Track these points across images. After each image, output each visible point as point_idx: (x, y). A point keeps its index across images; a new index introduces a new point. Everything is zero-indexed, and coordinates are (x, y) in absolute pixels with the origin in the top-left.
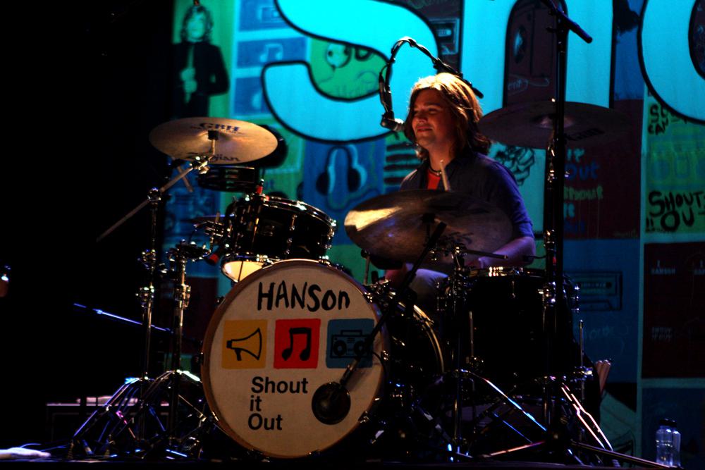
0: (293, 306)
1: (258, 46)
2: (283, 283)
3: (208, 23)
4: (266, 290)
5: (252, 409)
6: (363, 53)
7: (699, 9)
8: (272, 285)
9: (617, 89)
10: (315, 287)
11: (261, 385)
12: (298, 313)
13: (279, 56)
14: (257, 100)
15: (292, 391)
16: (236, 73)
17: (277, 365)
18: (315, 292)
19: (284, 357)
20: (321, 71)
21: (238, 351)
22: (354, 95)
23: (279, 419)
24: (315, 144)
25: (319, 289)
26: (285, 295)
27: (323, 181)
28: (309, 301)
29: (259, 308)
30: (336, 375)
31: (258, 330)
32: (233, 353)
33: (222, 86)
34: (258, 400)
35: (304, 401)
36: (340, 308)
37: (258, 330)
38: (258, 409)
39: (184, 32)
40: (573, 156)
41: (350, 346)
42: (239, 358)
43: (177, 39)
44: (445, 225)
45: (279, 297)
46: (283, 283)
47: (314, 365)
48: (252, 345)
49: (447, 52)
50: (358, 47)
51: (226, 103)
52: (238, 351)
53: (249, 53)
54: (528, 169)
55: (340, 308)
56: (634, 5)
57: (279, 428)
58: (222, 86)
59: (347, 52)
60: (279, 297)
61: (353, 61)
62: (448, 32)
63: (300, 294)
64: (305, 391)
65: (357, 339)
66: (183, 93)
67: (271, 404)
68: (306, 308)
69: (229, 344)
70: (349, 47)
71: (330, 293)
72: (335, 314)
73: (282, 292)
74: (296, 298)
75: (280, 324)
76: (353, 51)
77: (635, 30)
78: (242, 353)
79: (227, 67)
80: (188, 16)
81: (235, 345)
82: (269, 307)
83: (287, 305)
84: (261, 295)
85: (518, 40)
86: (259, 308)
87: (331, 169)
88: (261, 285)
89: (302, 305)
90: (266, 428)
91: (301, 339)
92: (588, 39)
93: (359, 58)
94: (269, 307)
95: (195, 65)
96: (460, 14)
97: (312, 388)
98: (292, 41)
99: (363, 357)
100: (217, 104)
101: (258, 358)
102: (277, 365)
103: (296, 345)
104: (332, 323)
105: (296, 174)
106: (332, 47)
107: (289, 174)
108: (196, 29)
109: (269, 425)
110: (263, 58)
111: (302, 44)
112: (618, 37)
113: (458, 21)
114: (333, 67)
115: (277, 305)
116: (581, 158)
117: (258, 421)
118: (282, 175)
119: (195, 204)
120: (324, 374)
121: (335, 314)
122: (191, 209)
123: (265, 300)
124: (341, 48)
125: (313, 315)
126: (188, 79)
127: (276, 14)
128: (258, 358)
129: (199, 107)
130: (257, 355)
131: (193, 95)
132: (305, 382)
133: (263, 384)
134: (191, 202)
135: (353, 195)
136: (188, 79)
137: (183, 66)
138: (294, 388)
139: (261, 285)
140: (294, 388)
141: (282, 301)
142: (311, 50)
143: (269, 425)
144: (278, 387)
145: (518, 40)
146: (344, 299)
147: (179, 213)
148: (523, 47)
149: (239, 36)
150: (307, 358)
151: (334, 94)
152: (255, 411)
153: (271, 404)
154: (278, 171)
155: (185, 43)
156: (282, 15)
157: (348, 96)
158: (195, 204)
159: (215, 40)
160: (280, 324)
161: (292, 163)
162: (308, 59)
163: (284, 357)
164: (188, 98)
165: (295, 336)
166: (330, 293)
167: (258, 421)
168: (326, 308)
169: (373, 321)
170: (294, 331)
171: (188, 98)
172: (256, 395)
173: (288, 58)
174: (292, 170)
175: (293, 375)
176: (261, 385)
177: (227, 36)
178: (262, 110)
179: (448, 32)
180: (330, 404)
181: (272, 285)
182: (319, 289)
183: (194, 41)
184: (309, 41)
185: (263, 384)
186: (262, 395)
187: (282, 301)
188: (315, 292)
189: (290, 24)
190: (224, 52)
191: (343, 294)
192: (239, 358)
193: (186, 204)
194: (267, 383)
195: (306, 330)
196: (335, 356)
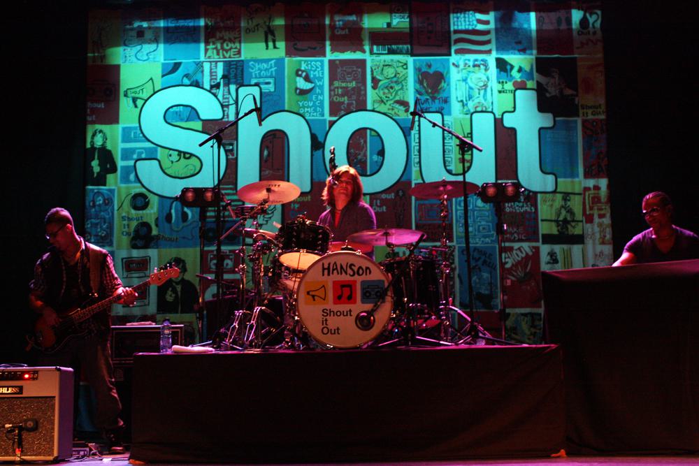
0: (341, 274)
1: (133, 151)
2: (335, 263)
3: (105, 138)
4: (326, 266)
5: (323, 324)
6: (188, 156)
7: (351, 142)
8: (329, 264)
9: (314, 177)
10: (352, 265)
11: (327, 313)
12: (344, 278)
13: (143, 156)
14: (132, 177)
15: (344, 316)
16: (120, 164)
17: (335, 303)
18: (353, 267)
19: (338, 299)
20: (166, 164)
21: (313, 296)
22: (183, 176)
23: (338, 329)
24: (165, 199)
25: (354, 266)
26: (337, 269)
27: (168, 218)
28: (350, 271)
29: (323, 275)
30: (368, 307)
31: (324, 286)
32: (311, 297)
33: (113, 169)
34: (326, 320)
35: (351, 320)
36: (366, 274)
37: (324, 286)
38: (326, 324)
39: (92, 143)
40: (294, 207)
41: (374, 293)
42: (314, 300)
43: (88, 146)
44: (544, 236)
45: (333, 270)
46: (335, 263)
47: (355, 302)
48: (321, 293)
49: (230, 157)
50: (185, 153)
51: (116, 178)
52: (313, 296)
53: (127, 154)
54: (273, 212)
55: (366, 274)
56: (321, 139)
57: (339, 334)
58: (113, 169)
59: (179, 155)
60: (333, 270)
61: (182, 159)
62: (231, 147)
63: (345, 267)
64: (351, 315)
65: (377, 290)
66: (93, 173)
67: (333, 322)
68: (348, 275)
69: (308, 293)
70: (180, 152)
71: (360, 268)
72: (364, 277)
73: (335, 267)
74: (342, 270)
75: (335, 283)
76: (182, 155)
77: (321, 150)
78: (316, 297)
79: (115, 160)
80: (94, 135)
81: (311, 293)
82: (329, 274)
83: (338, 274)
84: (324, 269)
85: (266, 153)
86: (323, 275)
87: (173, 211)
88: (323, 264)
89: (346, 273)
90: (331, 333)
91: (346, 290)
92: (481, 151)
93: (185, 158)
94: (329, 274)
95: (98, 159)
96: (237, 139)
97: (354, 314)
98: (150, 149)
99: (381, 296)
100: (110, 178)
101: (324, 300)
102: (335, 303)
103: (344, 293)
104: (363, 282)
105: (154, 213)
106: (171, 152)
107: (151, 214)
108: (98, 141)
109: (333, 332)
110: (135, 157)
111: (156, 151)
112: (314, 153)
113: (235, 142)
114: (172, 162)
115: (333, 273)
116: (298, 208)
117: (326, 330)
118: (147, 214)
119: (101, 227)
120: (360, 307)
121: (364, 277)
122: (99, 230)
123: (326, 272)
124: (177, 153)
125: (353, 278)
126: (95, 164)
127: (141, 135)
128: (324, 300)
129: (101, 180)
130: (323, 297)
131: (98, 173)
132: (350, 311)
133: (328, 312)
134: (99, 226)
135: (185, 224)
136: (95, 164)
137: (93, 159)
138: (345, 314)
139: (323, 264)
140: (345, 314)
141: (335, 271)
142: (160, 153)
143: (333, 332)
144: (335, 314)
145: (266, 153)
146: (368, 271)
147: (94, 232)
148: (268, 155)
149: (121, 146)
150: (351, 299)
151: (173, 175)
152: (325, 325)
153: (333, 322)
154: (144, 212)
155: (93, 148)
156: (144, 136)
157: (180, 176)
158: (101, 227)
159: (109, 147)
160: (335, 283)
161: (152, 208)
162: (159, 158)
163: (338, 299)
164: (95, 175)
165: (343, 289)
166: (360, 268)
167: (326, 330)
168: (358, 274)
169: (383, 281)
170: (343, 286)
171: (95, 175)
172: (325, 318)
173: (148, 157)
174: (152, 211)
175: (344, 307)
176: (327, 313)
177: (116, 146)
178: (135, 182)
179: (231, 147)
180: (364, 322)
181: (329, 264)
182: (354, 266)
183: (98, 147)
184: (159, 148)
185: (328, 312)
186: (328, 317)
187: (335, 271)
188: (353, 267)
189: (149, 141)
190: (113, 152)
191: (367, 268)
192: (314, 300)
193: (97, 228)
194: (330, 312)
195: (350, 286)
196: (366, 296)
